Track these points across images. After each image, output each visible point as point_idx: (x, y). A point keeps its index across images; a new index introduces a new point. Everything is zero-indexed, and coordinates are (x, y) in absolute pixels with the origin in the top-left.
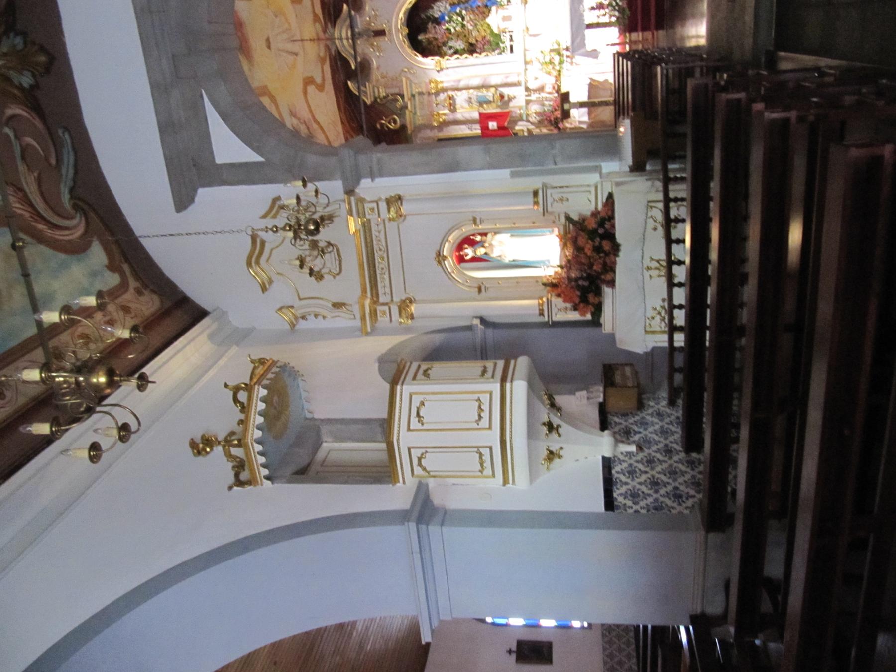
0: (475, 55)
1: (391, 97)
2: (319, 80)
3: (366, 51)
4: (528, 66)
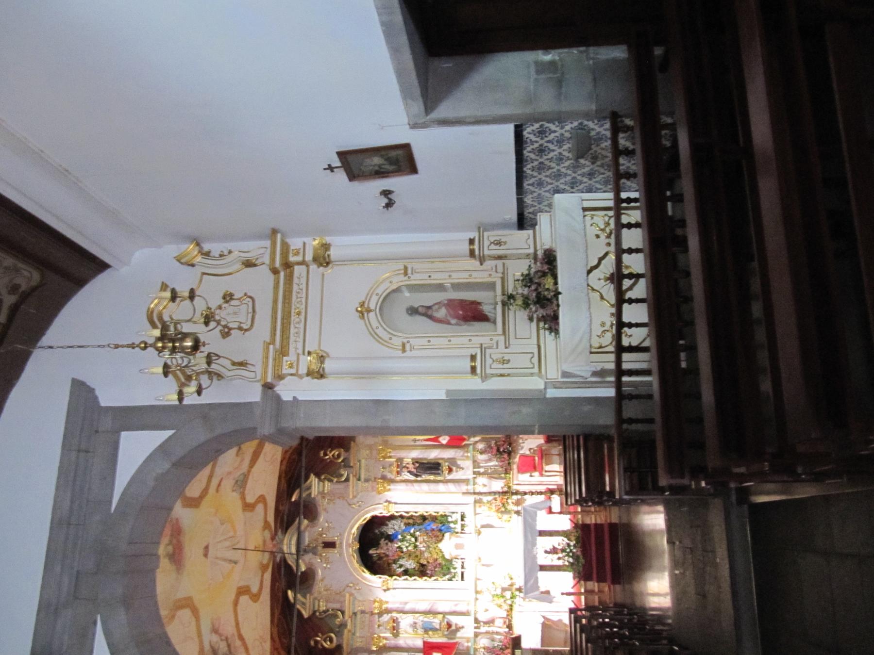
0: (425, 578)
1: (331, 612)
2: (255, 589)
3: (313, 561)
4: (479, 596)
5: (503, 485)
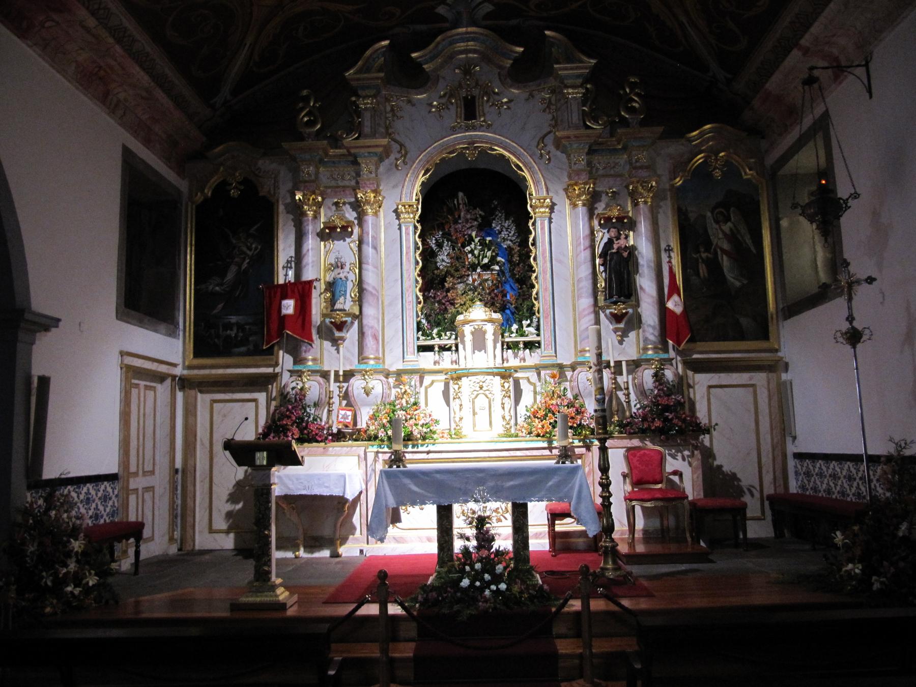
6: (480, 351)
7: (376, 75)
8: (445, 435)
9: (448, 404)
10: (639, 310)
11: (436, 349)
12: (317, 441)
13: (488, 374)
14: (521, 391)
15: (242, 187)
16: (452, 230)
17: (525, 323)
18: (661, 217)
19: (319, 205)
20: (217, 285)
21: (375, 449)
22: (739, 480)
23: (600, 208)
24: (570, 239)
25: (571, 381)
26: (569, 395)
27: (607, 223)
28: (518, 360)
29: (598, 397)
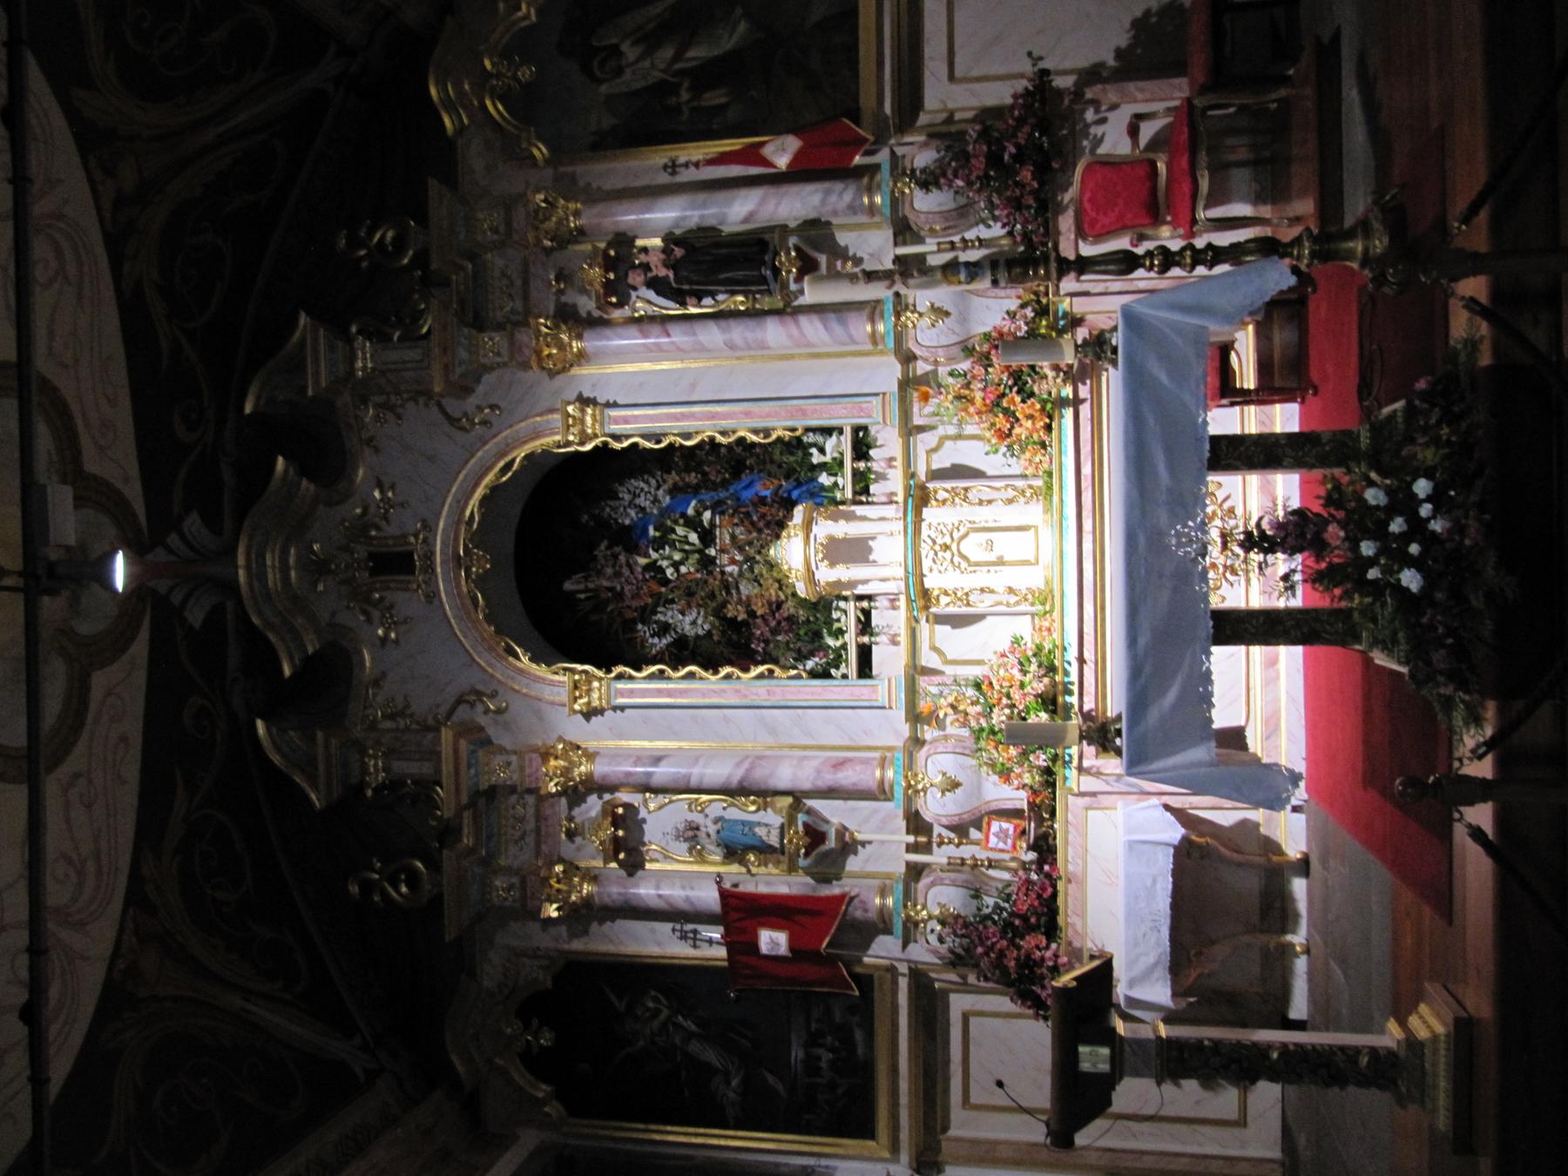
5: (1013, 304)
6: (870, 550)
7: (320, 750)
8: (1046, 624)
9: (979, 618)
10: (793, 224)
11: (866, 639)
12: (1054, 895)
13: (917, 531)
14: (954, 466)
15: (535, 1022)
16: (635, 604)
17: (816, 458)
18: (608, 185)
19: (572, 868)
20: (728, 1083)
21: (1072, 773)
22: (1147, 13)
23: (586, 305)
24: (647, 366)
25: (936, 363)
26: (965, 366)
27: (618, 291)
28: (891, 473)
29: (962, 277)
